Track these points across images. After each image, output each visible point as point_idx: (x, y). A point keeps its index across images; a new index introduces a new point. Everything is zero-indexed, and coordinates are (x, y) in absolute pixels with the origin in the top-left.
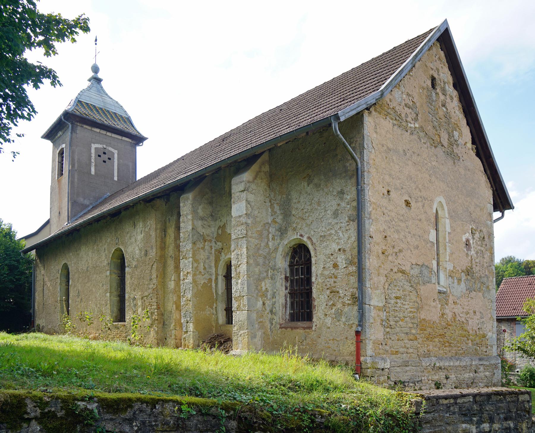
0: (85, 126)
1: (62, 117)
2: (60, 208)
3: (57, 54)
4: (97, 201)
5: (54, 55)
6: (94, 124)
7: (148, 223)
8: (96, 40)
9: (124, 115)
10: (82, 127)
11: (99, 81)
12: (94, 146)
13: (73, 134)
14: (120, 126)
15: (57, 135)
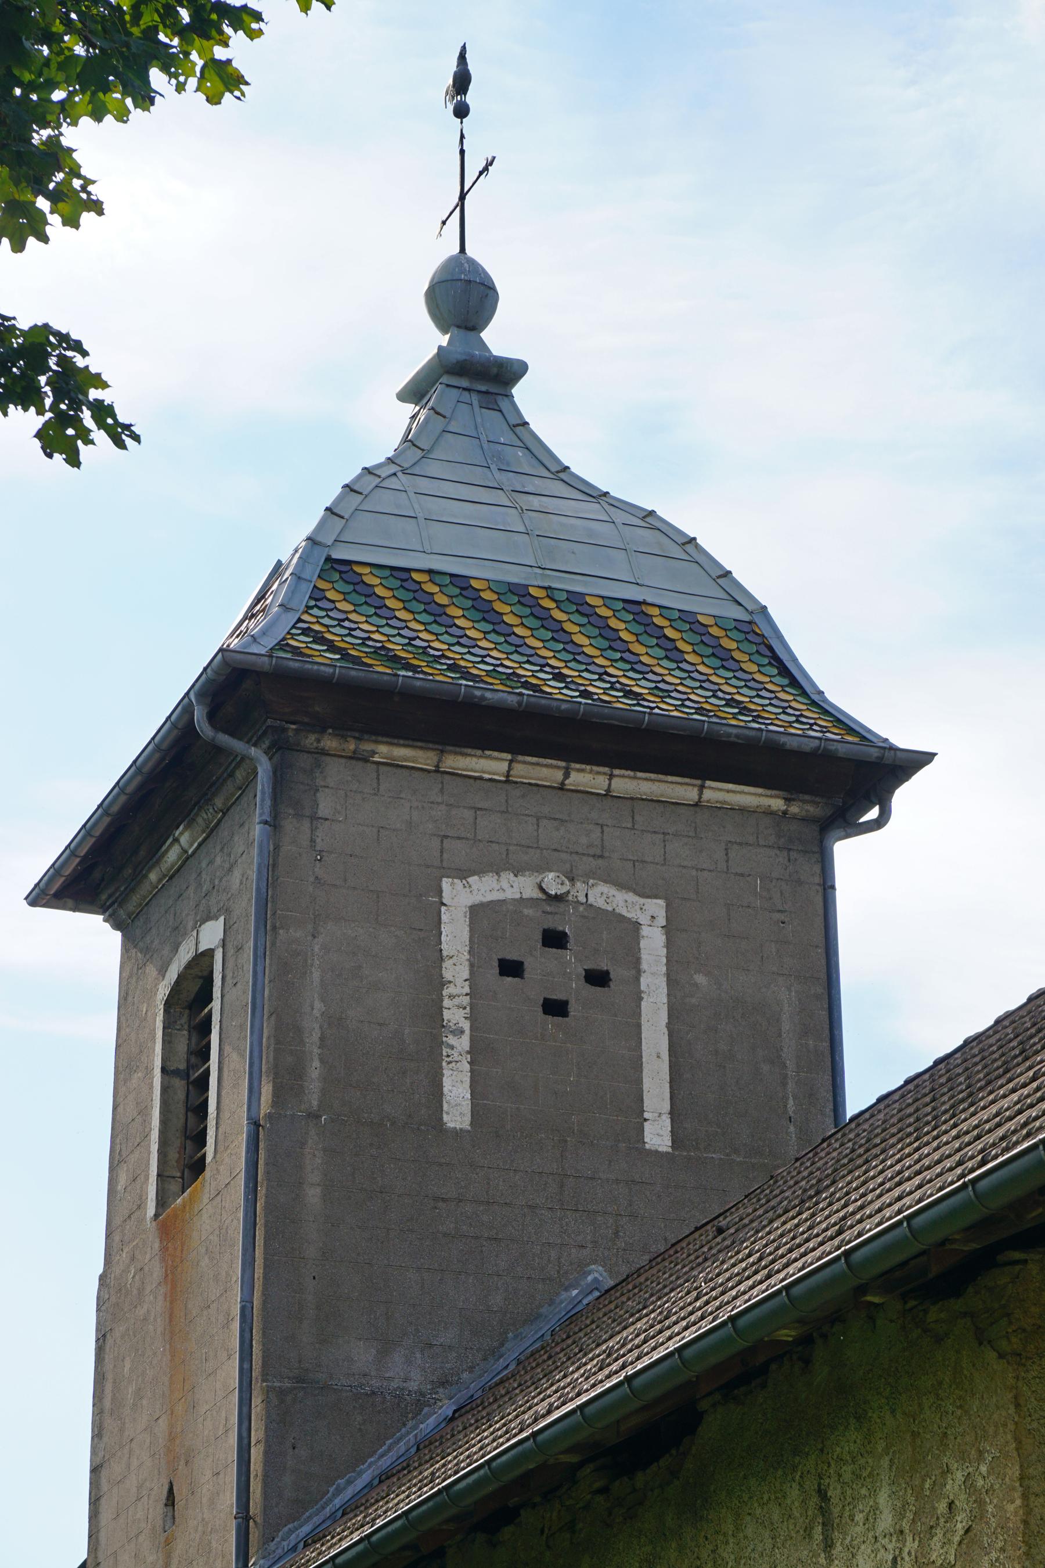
0: (384, 751)
1: (199, 714)
2: (177, 1454)
3: (97, 207)
4: (495, 1353)
5: (72, 222)
6: (457, 721)
7: (953, 1486)
8: (462, 82)
9: (706, 609)
10: (361, 758)
11: (496, 378)
12: (459, 897)
13: (289, 825)
14: (678, 695)
15: (155, 854)
